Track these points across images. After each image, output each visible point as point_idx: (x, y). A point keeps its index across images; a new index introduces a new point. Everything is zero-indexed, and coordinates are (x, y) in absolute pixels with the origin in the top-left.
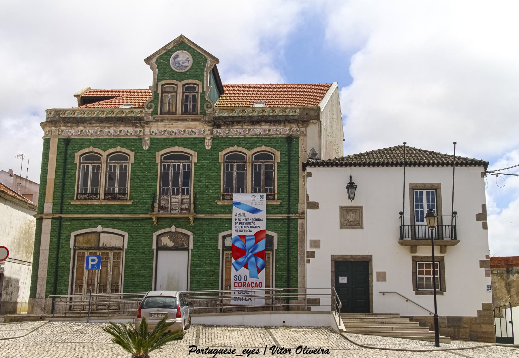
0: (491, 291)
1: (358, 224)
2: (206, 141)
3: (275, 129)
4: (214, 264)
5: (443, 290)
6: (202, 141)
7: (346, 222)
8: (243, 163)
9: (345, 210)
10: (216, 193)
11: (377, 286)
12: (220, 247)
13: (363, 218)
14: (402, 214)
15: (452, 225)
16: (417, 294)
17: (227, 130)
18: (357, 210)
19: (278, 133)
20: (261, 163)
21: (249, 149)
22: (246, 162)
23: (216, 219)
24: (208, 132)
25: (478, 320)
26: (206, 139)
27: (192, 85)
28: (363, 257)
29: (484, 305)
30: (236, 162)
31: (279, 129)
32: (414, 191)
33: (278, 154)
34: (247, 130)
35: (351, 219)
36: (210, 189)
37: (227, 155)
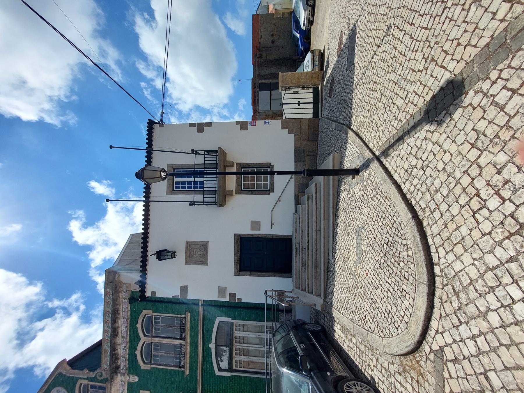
0: (269, 121)
1: (204, 247)
2: (131, 381)
3: (123, 313)
4: (245, 382)
5: (269, 165)
6: (130, 384)
7: (201, 259)
8: (153, 346)
9: (190, 260)
10: (179, 374)
11: (265, 231)
12: (228, 374)
13: (197, 242)
14: (192, 204)
15: (205, 154)
16: (273, 191)
17: (122, 359)
18: (190, 246)
19: (127, 310)
20: (153, 328)
21: (139, 339)
22: (152, 343)
23: (202, 377)
24: (123, 378)
25: (298, 133)
26: (129, 380)
27: (82, 388)
28: (236, 243)
29: (283, 128)
30: (151, 352)
31: (124, 309)
32: (175, 190)
33: (145, 312)
34: (122, 339)
35: (199, 253)
36: (175, 379)
37: (145, 360)
